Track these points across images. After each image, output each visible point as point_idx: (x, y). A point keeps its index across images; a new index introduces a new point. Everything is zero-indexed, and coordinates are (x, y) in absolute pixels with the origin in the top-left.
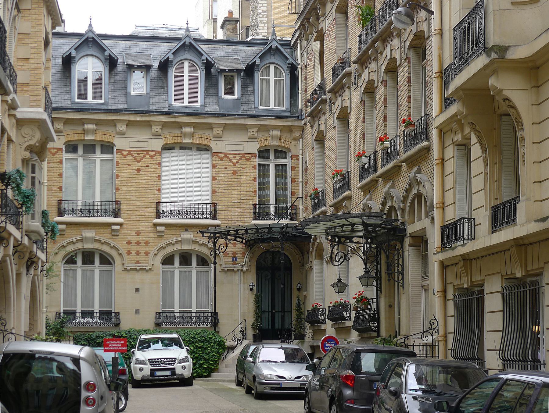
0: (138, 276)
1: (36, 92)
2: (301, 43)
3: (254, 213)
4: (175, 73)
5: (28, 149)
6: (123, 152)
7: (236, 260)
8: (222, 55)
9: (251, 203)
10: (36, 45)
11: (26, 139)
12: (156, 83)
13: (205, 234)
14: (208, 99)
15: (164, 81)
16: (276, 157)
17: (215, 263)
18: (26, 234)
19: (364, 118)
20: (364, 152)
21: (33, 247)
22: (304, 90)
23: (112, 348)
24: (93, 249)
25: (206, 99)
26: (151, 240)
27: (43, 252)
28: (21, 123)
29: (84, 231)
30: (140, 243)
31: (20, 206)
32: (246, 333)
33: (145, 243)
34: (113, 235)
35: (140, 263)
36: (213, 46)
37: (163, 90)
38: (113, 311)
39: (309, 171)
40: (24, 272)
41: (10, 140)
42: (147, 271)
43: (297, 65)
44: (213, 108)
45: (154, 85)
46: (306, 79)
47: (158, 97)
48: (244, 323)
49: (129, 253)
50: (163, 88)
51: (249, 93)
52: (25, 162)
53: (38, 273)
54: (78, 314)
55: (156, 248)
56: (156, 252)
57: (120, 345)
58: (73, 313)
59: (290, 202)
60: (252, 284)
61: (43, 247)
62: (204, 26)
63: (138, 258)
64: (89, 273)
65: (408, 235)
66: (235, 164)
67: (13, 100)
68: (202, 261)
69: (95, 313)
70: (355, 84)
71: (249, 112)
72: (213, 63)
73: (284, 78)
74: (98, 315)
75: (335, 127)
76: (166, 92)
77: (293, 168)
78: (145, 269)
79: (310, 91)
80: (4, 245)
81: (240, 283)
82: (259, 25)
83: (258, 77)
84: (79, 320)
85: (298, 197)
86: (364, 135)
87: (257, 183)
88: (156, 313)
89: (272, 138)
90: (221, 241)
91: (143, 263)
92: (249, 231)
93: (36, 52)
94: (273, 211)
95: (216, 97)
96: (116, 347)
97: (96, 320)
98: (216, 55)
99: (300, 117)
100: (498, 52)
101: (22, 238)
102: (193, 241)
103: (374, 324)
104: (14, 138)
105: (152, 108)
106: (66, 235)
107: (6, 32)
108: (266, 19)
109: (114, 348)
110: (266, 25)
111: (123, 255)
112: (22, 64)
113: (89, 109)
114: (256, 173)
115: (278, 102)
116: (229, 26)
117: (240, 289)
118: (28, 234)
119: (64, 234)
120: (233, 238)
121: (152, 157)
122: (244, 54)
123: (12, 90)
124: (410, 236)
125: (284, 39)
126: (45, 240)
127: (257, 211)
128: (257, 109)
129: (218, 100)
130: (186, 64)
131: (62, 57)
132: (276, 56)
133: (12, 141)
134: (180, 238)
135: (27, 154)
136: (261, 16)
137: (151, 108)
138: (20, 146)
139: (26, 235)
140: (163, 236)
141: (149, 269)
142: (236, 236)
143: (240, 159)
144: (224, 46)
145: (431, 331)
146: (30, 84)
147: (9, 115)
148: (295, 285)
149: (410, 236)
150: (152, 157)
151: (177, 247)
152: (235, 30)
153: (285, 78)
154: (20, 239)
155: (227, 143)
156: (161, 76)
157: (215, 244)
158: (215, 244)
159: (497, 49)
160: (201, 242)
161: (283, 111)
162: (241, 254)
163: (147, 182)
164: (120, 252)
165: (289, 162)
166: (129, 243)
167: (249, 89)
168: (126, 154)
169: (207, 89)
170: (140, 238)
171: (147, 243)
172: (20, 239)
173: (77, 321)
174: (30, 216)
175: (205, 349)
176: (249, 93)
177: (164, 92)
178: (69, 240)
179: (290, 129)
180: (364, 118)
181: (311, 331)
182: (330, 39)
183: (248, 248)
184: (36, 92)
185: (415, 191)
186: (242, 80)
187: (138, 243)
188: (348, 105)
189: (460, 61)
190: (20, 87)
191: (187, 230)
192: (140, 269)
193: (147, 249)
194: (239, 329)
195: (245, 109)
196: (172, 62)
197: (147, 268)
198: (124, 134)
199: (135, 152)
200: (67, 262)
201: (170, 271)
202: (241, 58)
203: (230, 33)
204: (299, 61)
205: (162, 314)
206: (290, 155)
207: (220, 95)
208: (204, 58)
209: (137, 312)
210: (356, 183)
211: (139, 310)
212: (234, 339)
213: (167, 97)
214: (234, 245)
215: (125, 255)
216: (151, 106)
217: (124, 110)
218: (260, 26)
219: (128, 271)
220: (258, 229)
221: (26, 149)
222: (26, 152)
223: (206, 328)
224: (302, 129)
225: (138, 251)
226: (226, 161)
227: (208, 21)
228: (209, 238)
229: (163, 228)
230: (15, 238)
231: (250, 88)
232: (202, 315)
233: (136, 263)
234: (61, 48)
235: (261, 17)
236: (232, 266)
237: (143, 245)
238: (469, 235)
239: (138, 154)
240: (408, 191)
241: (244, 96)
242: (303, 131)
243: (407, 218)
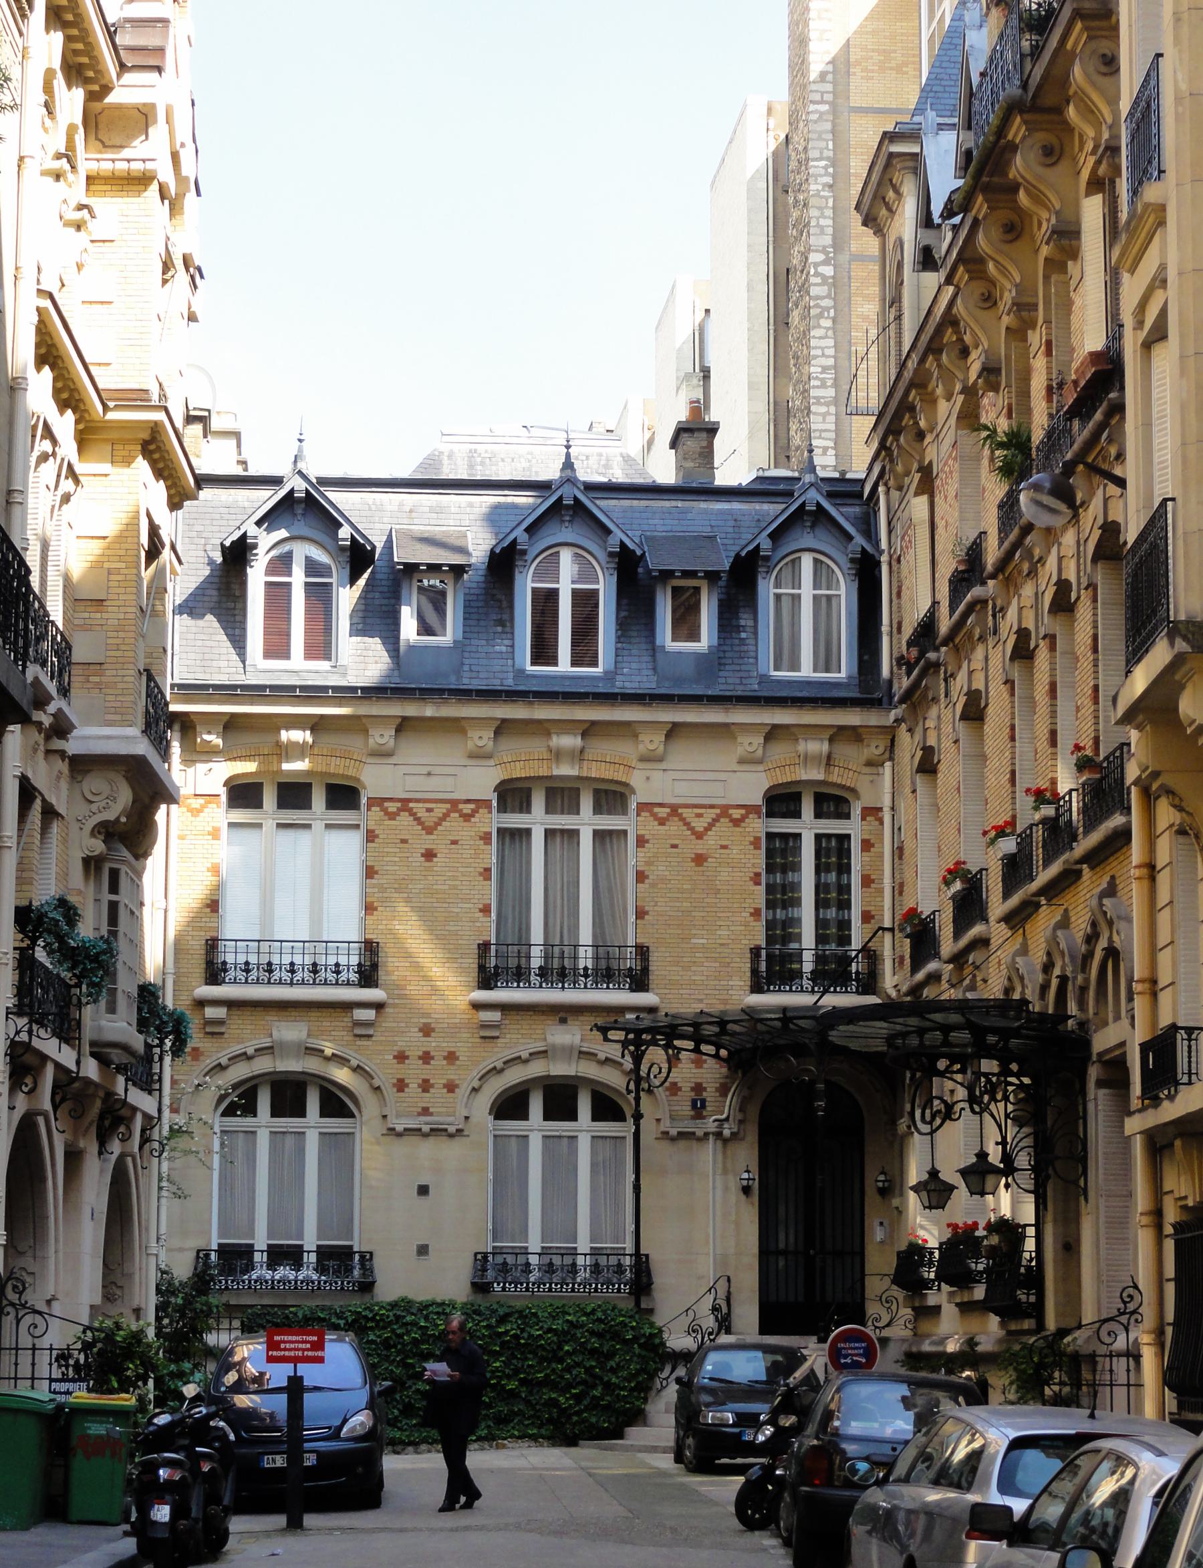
0: (427, 1150)
1: (120, 686)
2: (887, 493)
3: (755, 972)
4: (533, 581)
5: (99, 833)
6: (386, 804)
7: (703, 1106)
8: (669, 528)
9: (747, 943)
10: (123, 565)
11: (94, 807)
12: (481, 610)
13: (612, 1035)
14: (626, 653)
15: (505, 604)
16: (818, 815)
17: (638, 1117)
18: (95, 1050)
19: (1013, 728)
20: (1012, 823)
21: (114, 1082)
22: (895, 626)
23: (287, 1353)
24: (303, 1073)
25: (620, 652)
26: (463, 1054)
27: (150, 1093)
28: (81, 765)
29: (277, 1023)
30: (433, 1058)
31: (74, 981)
32: (729, 1314)
33: (445, 1058)
34: (356, 1036)
35: (431, 1114)
36: (643, 503)
37: (499, 629)
38: (355, 1249)
39: (907, 852)
40: (93, 1148)
41: (50, 813)
42: (451, 1136)
43: (876, 554)
44: (638, 679)
45: (476, 616)
46: (899, 595)
47: (486, 649)
48: (723, 1282)
49: (401, 1085)
50: (501, 623)
51: (743, 635)
52: (92, 864)
53: (133, 1147)
54: (257, 1257)
55: (476, 1073)
56: (476, 1084)
57: (308, 1346)
58: (246, 1252)
59: (856, 943)
60: (746, 1176)
61: (151, 1075)
62: (678, 389)
63: (426, 1100)
64: (290, 1140)
65: (1094, 1058)
66: (699, 836)
67: (59, 715)
68: (606, 1109)
69: (305, 1254)
70: (995, 634)
71: (741, 688)
72: (639, 553)
73: (842, 591)
74: (313, 1258)
75: (956, 742)
76: (509, 636)
77: (867, 845)
78: (446, 1130)
79: (908, 631)
80: (25, 1089)
81: (714, 1174)
82: (813, 408)
83: (767, 589)
84: (261, 1272)
85: (881, 928)
86: (1013, 773)
87: (763, 888)
88: (476, 1254)
89: (806, 759)
90: (656, 1055)
91: (439, 1114)
92: (730, 1027)
93: (122, 584)
94: (808, 967)
95: (649, 647)
96: (298, 1349)
97: (308, 1272)
98: (652, 528)
99: (885, 700)
100: (1190, 636)
101: (78, 1063)
102: (580, 1052)
103: (1028, 1295)
104: (61, 810)
105: (468, 682)
106: (226, 1036)
107: (28, 572)
108: (831, 392)
109: (292, 1353)
110: (832, 409)
111: (385, 1092)
112: (86, 615)
113: (293, 688)
114: (759, 860)
115: (826, 660)
116: (691, 443)
117: (714, 1188)
118: (100, 1052)
119: (222, 1034)
120: (690, 1045)
121: (467, 817)
122: (732, 523)
123: (54, 692)
124: (1099, 1061)
125: (848, 476)
126: (156, 1058)
127: (763, 966)
128: (764, 679)
129: (654, 656)
130: (566, 556)
131: (222, 545)
132: (821, 532)
133: (58, 815)
134: (543, 1044)
135: (98, 846)
136: (817, 383)
137: (465, 681)
138: (80, 824)
139: (93, 1055)
140: (497, 1037)
141: (458, 1130)
142: (699, 1040)
143: (715, 820)
144: (674, 503)
145: (1124, 1319)
146: (104, 667)
147: (48, 752)
148: (873, 1179)
149: (1099, 1061)
150: (467, 817)
151: (537, 1069)
152: (706, 457)
153: (844, 591)
154: (74, 1069)
155: (678, 775)
156: (495, 592)
157: (638, 1059)
158: (638, 1059)
159: (1187, 628)
160: (602, 1056)
161: (836, 685)
162: (717, 1090)
163: (455, 887)
164: (376, 1083)
165: (854, 827)
166: (401, 1057)
167: (742, 622)
168: (395, 810)
169: (623, 626)
170: (431, 1044)
171: (451, 1057)
172: (74, 1069)
173: (254, 1277)
174: (103, 1003)
175: (611, 1355)
176: (743, 635)
177: (504, 636)
178: (237, 1049)
179: (853, 734)
180: (1013, 728)
181: (909, 1311)
182: (946, 497)
183: (736, 1072)
184: (120, 686)
185: (1103, 943)
186: (722, 596)
187: (426, 1057)
188: (982, 687)
189: (1134, 641)
190: (81, 672)
191: (563, 1021)
192: (432, 1130)
193: (452, 1074)
194: (708, 1301)
195: (730, 681)
196: (524, 552)
197: (452, 1129)
198: (389, 754)
199: (421, 805)
200: (229, 1112)
201: (518, 1136)
202: (723, 535)
203: (692, 465)
204: (884, 545)
205: (490, 1258)
206: (856, 810)
207: (658, 642)
208: (613, 543)
209: (423, 1250)
210: (997, 906)
211: (427, 1246)
212: (692, 1330)
213: (509, 649)
214: (698, 1064)
215: (390, 1092)
216: (465, 674)
217: (392, 689)
218: (815, 414)
219: (399, 1135)
220: (751, 1014)
221: (93, 834)
222: (93, 840)
223: (619, 1297)
224: (890, 734)
225: (426, 1081)
226: (674, 827)
227: (687, 377)
228: (625, 1044)
229: (495, 1016)
230: (58, 1066)
231: (745, 620)
232: (603, 1261)
233: (419, 1114)
234: (222, 519)
235: (817, 387)
236: (691, 1123)
237: (438, 1062)
238: (1190, 1070)
239: (429, 810)
240: (1092, 938)
241: (728, 641)
242: (893, 741)
243: (1091, 1011)
